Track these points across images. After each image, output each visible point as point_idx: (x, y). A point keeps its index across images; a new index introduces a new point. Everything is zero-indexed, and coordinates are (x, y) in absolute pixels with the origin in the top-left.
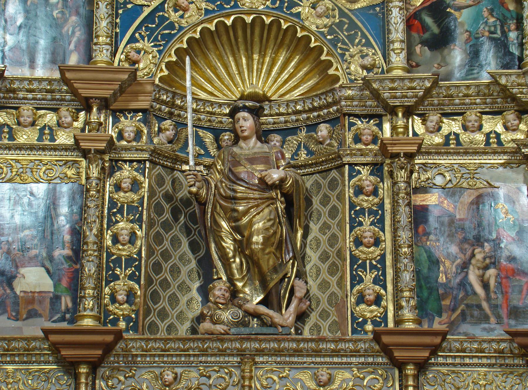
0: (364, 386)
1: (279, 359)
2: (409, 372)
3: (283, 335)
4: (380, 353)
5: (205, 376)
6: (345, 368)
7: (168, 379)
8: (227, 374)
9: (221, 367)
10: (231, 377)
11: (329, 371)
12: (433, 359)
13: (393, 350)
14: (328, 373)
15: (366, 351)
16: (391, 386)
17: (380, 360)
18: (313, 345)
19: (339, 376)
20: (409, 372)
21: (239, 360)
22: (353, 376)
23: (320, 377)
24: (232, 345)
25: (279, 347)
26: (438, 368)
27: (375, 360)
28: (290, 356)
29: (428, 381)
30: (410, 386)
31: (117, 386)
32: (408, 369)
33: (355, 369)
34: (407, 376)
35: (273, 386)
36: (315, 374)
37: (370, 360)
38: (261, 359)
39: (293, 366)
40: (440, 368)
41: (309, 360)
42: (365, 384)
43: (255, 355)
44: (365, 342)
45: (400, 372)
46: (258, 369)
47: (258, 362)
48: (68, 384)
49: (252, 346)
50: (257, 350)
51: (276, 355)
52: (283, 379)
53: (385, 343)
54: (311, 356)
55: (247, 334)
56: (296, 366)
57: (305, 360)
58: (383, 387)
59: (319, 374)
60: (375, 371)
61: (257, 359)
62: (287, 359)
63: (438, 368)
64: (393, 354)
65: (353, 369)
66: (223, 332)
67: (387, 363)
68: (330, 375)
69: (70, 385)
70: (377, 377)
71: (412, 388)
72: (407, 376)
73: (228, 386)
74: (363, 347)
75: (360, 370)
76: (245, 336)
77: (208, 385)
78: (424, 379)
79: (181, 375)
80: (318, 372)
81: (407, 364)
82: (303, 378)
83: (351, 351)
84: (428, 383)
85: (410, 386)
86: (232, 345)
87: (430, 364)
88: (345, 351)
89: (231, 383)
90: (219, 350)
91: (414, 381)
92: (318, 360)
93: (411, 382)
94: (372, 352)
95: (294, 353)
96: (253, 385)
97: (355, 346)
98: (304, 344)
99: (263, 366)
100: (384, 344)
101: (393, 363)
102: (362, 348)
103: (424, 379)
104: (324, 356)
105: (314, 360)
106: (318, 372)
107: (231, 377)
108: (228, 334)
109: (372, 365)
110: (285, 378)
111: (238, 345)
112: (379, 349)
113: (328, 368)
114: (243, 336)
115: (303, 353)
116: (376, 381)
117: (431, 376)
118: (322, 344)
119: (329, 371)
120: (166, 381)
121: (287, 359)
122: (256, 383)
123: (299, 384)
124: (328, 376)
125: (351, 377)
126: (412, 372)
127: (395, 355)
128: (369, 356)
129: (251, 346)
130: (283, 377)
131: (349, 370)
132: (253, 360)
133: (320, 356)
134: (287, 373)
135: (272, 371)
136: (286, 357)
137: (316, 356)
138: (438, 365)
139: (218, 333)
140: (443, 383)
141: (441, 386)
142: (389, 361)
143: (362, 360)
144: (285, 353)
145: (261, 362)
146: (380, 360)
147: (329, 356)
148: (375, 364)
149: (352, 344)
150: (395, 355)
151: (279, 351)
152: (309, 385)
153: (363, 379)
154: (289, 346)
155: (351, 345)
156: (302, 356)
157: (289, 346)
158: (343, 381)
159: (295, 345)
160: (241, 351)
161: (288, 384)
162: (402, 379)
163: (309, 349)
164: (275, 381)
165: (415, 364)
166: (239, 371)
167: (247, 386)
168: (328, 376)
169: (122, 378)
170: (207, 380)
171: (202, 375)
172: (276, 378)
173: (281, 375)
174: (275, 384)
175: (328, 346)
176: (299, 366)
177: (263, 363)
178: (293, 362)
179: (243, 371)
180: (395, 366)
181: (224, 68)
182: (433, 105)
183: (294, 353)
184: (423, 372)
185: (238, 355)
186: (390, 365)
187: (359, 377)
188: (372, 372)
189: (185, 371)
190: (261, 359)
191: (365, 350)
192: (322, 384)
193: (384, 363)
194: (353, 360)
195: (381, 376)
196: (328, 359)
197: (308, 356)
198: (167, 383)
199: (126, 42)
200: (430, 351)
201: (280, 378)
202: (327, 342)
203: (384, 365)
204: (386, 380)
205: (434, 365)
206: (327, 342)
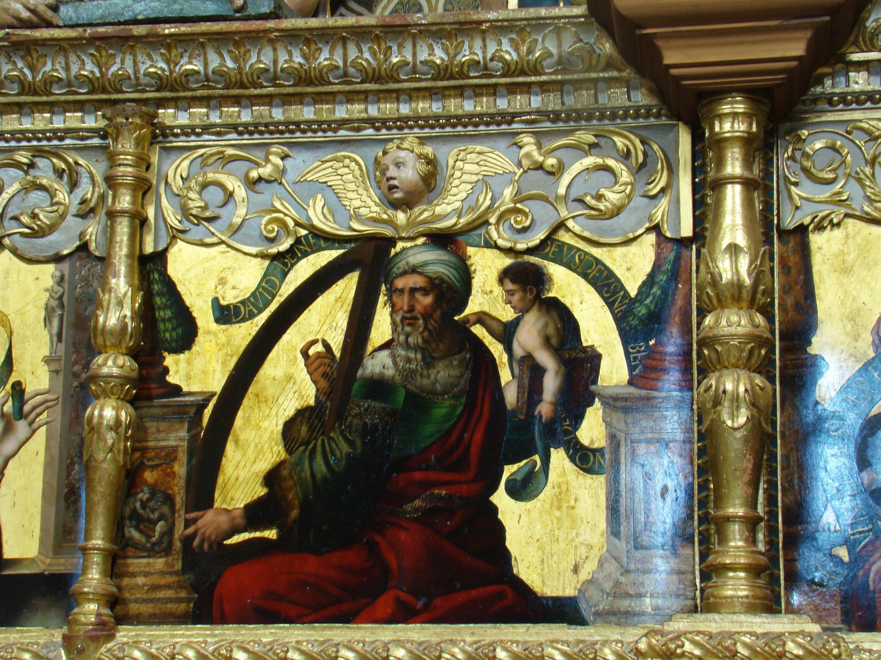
0: (557, 198)
1: (246, 117)
2: (727, 126)
3: (248, 18)
4: (619, 70)
6: (488, 136)
9: (39, 152)
10: (73, 185)
11: (428, 150)
12: (828, 82)
13: (660, 43)
14: (420, 156)
15: (564, 64)
16: (663, 191)
17: (617, 97)
18: (367, 55)
20: (726, 128)
21: (102, 123)
22: (519, 165)
23: (392, 172)
24: (67, 69)
25: (240, 69)
26: (847, 116)
27: (603, 99)
28: (287, 100)
29: (808, 164)
30: (732, 180)
32: (721, 117)
33: (527, 139)
34: (720, 143)
35: (223, 212)
36: (377, 161)
37: (581, 99)
38: (183, 119)
39: (298, 137)
40: (857, 115)
41: (356, 110)
42: (562, 191)
43: (162, 103)
44: (558, 31)
45: (697, 138)
46: (173, 156)
47: (172, 128)
49: (142, 68)
50: (162, 83)
51: (237, 101)
52: (262, 186)
53: (623, 12)
54: (364, 97)
55: (119, 23)
56: (309, 137)
57: (341, 112)
58: (629, 197)
59: (388, 160)
60: (602, 141)
61: (168, 116)
62: (278, 114)
63: (847, 116)
64: (659, 57)
65: (518, 139)
66: (25, 14)
67: (648, 109)
68: (431, 161)
70: (611, 162)
71: (738, 188)
72: (720, 143)
73: (63, 217)
74: (554, 51)
75: (544, 141)
76: (110, 30)
78: (792, 158)
80: (385, 153)
81: (719, 94)
82: (334, 181)
83: (509, 70)
84: (805, 171)
85: (732, 180)
86: (67, 69)
87: (815, 100)
88: (486, 70)
89: (73, 209)
90: (26, 88)
91: (748, 163)
92: (388, 108)
93: (734, 166)
94: (590, 69)
95: (299, 89)
96: (151, 212)
97: (524, 49)
98: (331, 52)
99: (193, 141)
100: (622, 18)
101: (669, 110)
102: (550, 55)
103: (792, 158)
104: (412, 95)
105: (373, 111)
106: (385, 153)
107: (73, 185)
108: (49, 25)
109: (589, 118)
110: (268, 182)
111: (90, 68)
112: (615, 54)
113: (423, 141)
114: (101, 30)
115: (329, 88)
116: (606, 176)
117: (818, 145)
118: (400, 46)
119: (428, 150)
121: (278, 114)
122: (164, 202)
123: (320, 203)
124: (422, 167)
125: (512, 167)
126: (741, 127)
127: (667, 61)
128: (577, 85)
129: (136, 71)
130: (260, 179)
131: (503, 143)
132: (150, 119)
133: (396, 95)
134: (276, 166)
135: (225, 161)
136: (270, 104)
137: (381, 96)
138: (846, 103)
139: (10, 20)
140: (868, 170)
141: (859, 181)
142: (654, 102)
143: (552, 102)
144: (264, 91)
145: (182, 127)
146: (617, 97)
147: (431, 93)
148: (602, 117)
149: (512, 40)
150: (667, 61)
151: (243, 86)
152: (357, 203)
153: (555, 173)
154: (275, 62)
155: (506, 46)
156: (331, 98)
157: (275, 62)
158: (484, 182)
159: (298, 59)
160: (104, 91)
161: (278, 205)
162: (704, 165)
163: (351, 70)
165: (752, 94)
167: (123, 212)
168: (422, 167)
172: (233, 184)
173: (254, 174)
174: (230, 206)
175: (423, 55)
176: (320, 137)
177: (188, 131)
178: (297, 124)
179: (112, 158)
180: (679, 119)
181: (664, 33)
183: (299, 89)
184: (789, 132)
185: (98, 105)
186: (658, 116)
187: (540, 167)
188: (593, 146)
190: (183, 119)
191: (560, 62)
192: (398, 195)
193: (637, 109)
194: (519, 102)
195: (626, 156)
196: (422, 106)
197: (350, 97)
200: (808, 34)
201: (252, 184)
202: (414, 37)
203: (637, 116)
204: (642, 169)
205: (830, 102)
206: (414, 37)
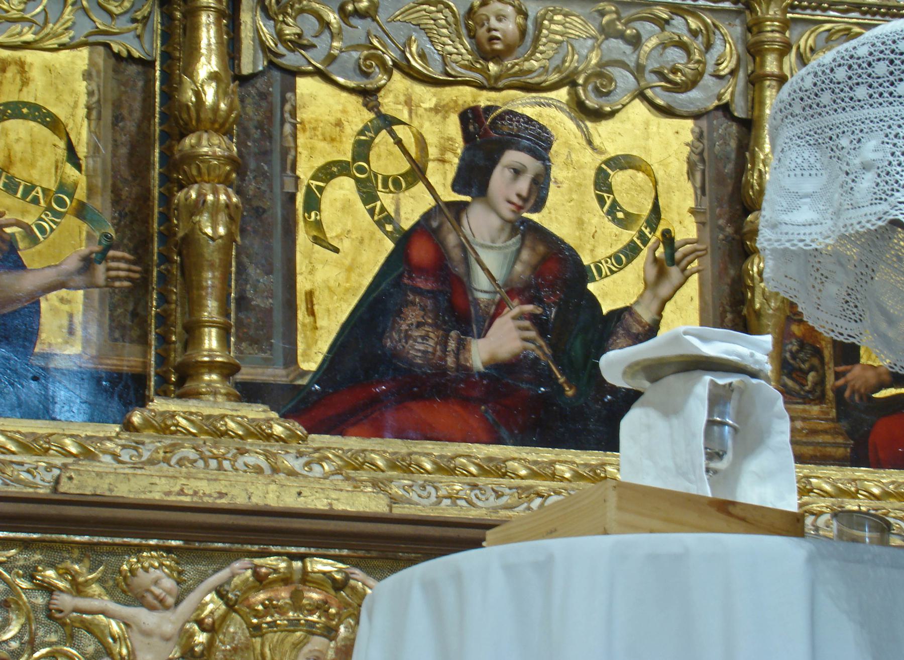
5: (621, 36)
7: (504, 33)
8: (694, 34)
19: (554, 27)
31: (315, 41)
48: (139, 15)
52: (355, 21)
69: (146, 19)
77: (632, 65)
79: (539, 26)
89: (710, 69)
120: (493, 39)
164: (327, 25)
166: (738, 29)
169: (333, 18)
170: (628, 49)
171: (607, 32)
182: (266, 567)
189: (555, 12)
198: (498, 46)
199: (49, 506)
